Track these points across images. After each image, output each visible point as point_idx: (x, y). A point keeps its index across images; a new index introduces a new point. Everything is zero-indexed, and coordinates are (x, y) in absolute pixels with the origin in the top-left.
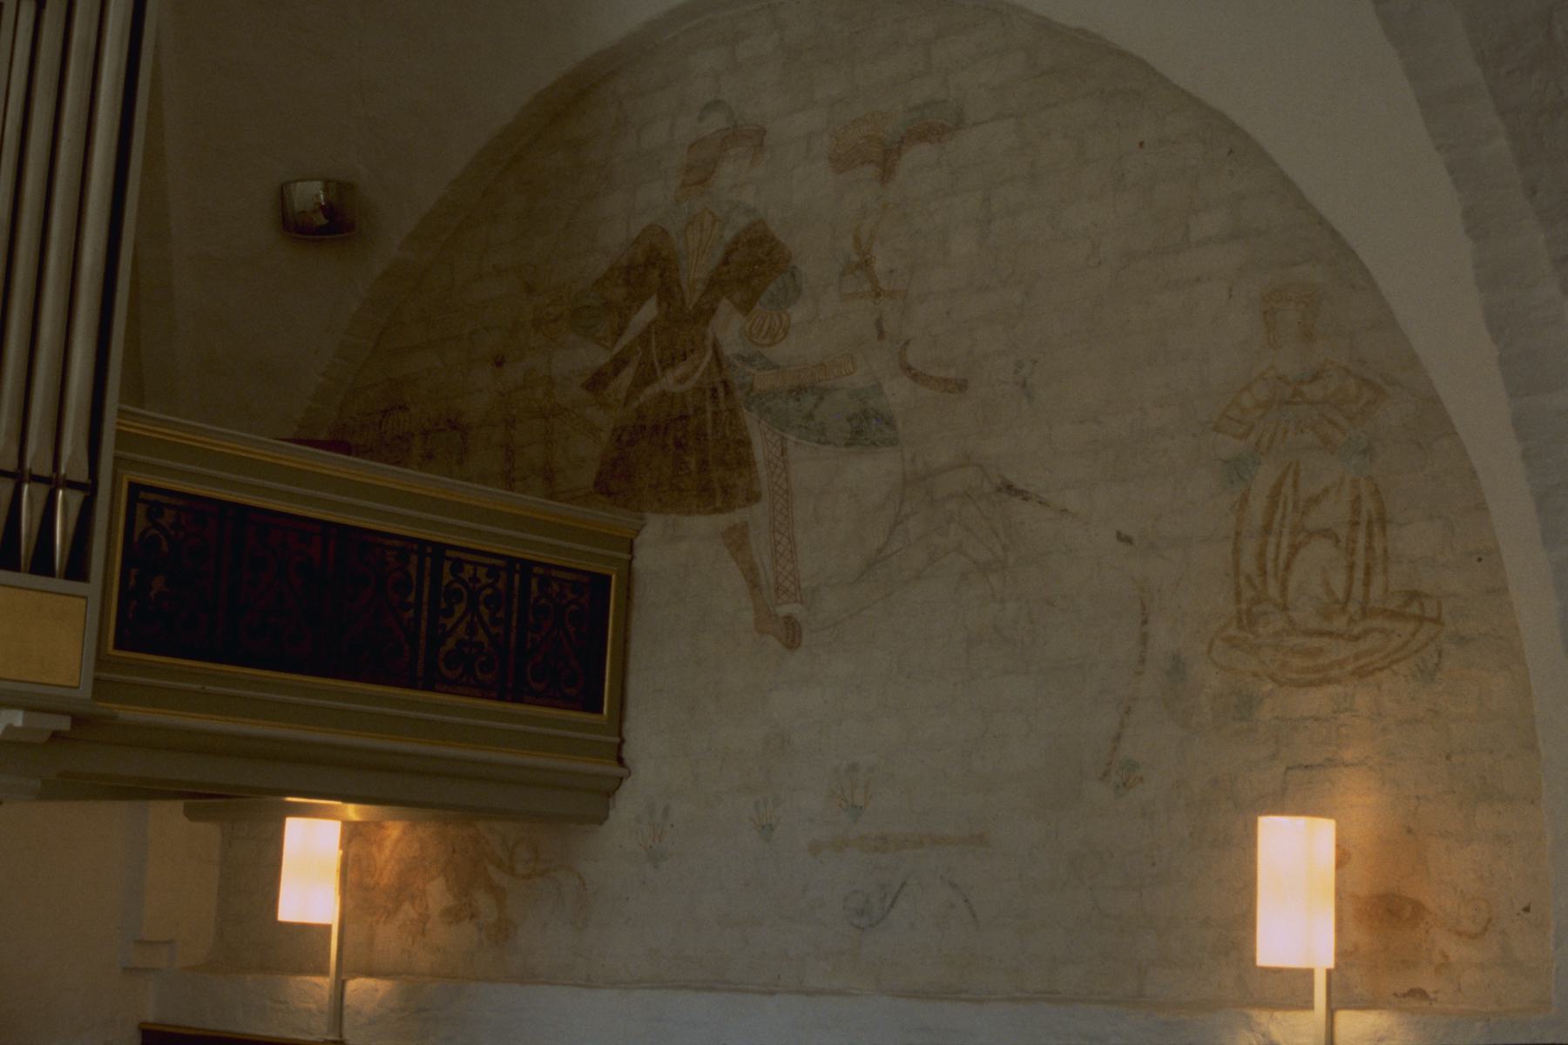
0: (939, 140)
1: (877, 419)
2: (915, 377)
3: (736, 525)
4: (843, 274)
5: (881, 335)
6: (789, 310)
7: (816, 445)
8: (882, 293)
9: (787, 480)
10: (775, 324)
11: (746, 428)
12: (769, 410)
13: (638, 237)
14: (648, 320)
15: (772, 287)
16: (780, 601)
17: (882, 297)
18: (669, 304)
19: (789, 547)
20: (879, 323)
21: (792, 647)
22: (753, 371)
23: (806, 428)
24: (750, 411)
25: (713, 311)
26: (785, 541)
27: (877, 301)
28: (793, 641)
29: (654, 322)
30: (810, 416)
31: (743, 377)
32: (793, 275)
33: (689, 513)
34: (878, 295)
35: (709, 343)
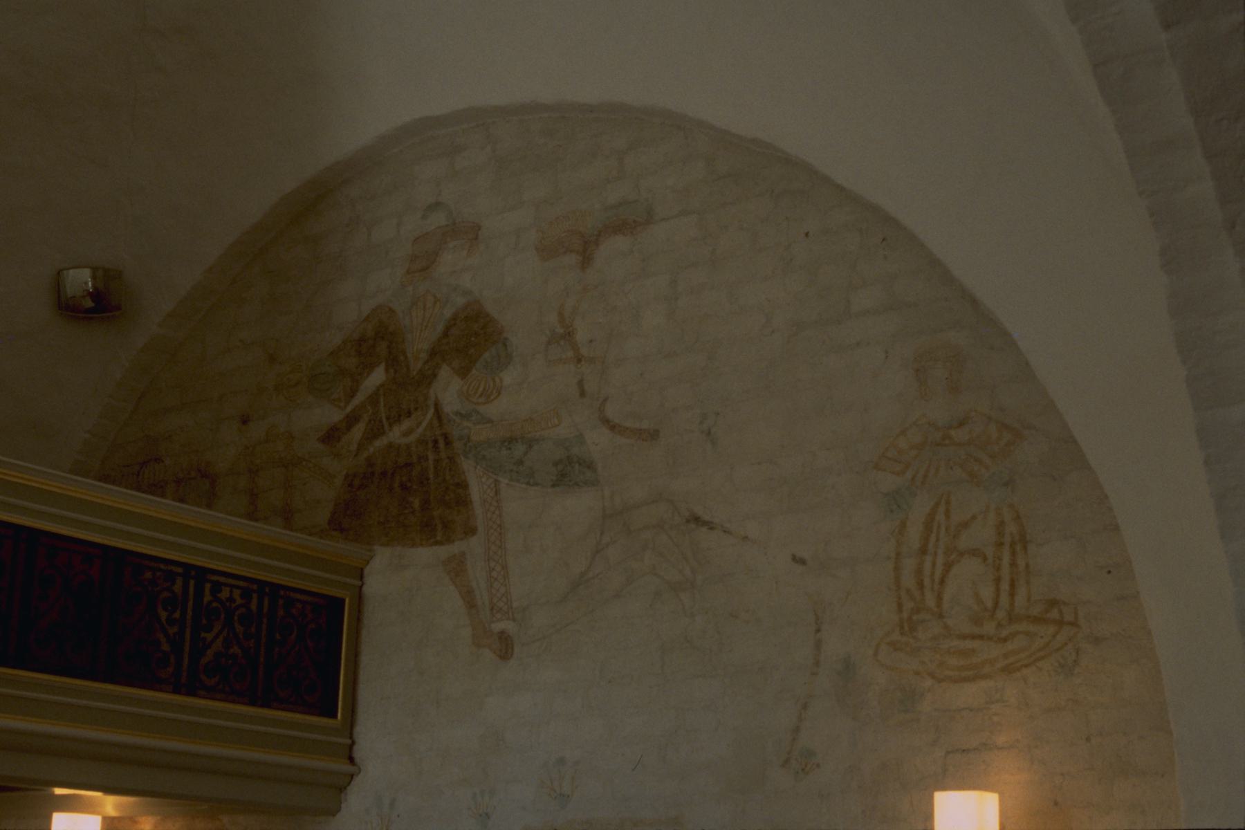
1: (580, 464)
2: (613, 428)
5: (583, 394)
7: (524, 486)
15: (487, 355)
17: (583, 363)
18: (396, 372)
20: (580, 384)
23: (517, 472)
25: (435, 376)
27: (579, 366)
29: (382, 385)
30: (520, 462)
32: (505, 345)
34: (579, 361)
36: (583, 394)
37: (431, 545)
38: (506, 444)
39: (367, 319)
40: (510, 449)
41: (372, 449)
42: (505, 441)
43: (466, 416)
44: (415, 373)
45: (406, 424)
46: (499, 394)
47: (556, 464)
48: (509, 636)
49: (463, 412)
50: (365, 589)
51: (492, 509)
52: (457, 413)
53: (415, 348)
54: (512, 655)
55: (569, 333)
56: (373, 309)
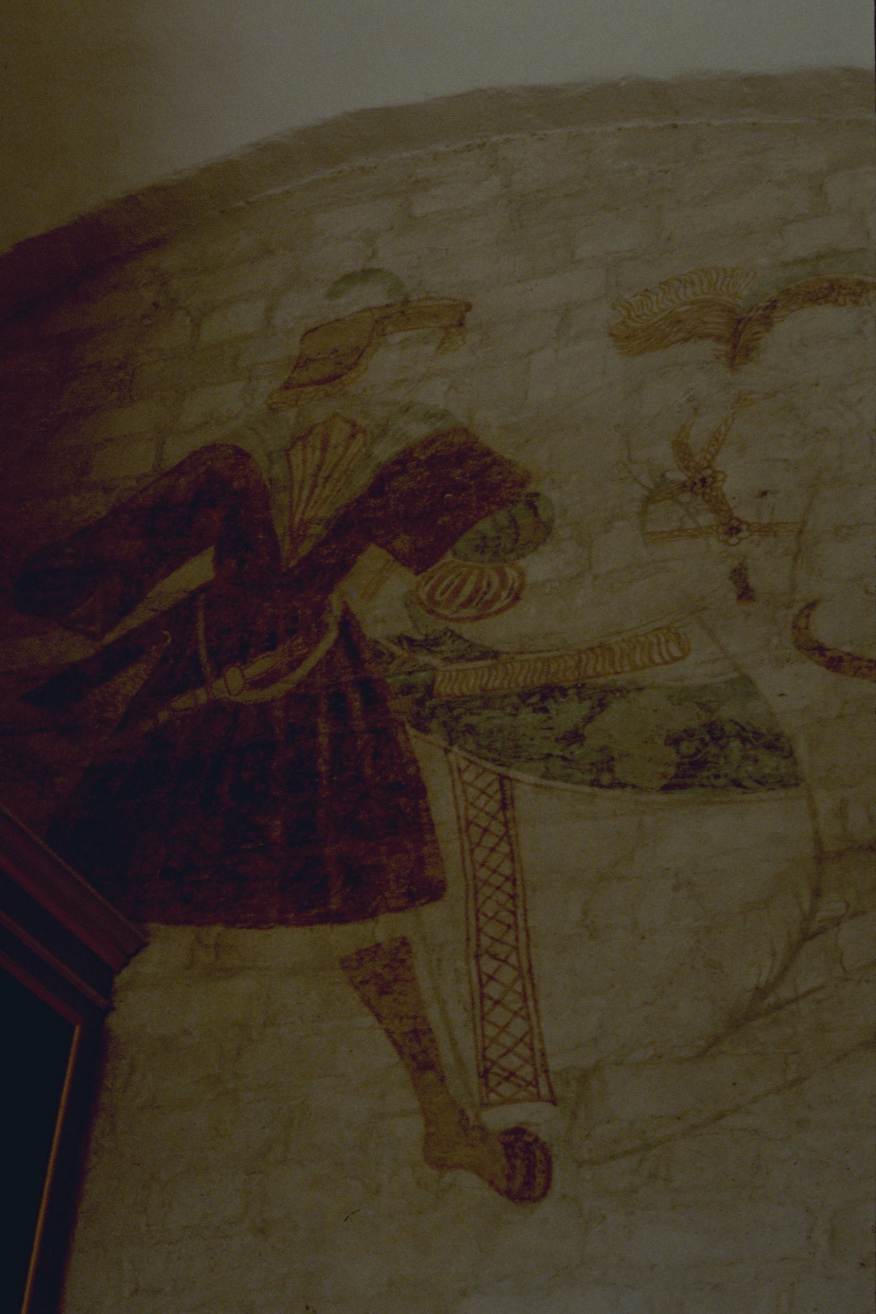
0: (856, 303)
1: (744, 740)
2: (835, 663)
3: (378, 945)
4: (649, 500)
5: (746, 594)
6: (522, 563)
7: (587, 789)
8: (744, 527)
9: (512, 857)
10: (489, 585)
11: (414, 761)
12: (470, 729)
13: (182, 464)
14: (193, 587)
15: (485, 526)
16: (493, 1097)
19: (518, 987)
20: (739, 575)
21: (522, 1199)
22: (435, 662)
23: (564, 758)
24: (426, 731)
26: (507, 974)
27: (734, 540)
28: (528, 1183)
29: (202, 589)
30: (576, 736)
31: (410, 673)
32: (532, 506)
33: (260, 922)
35: (332, 619)
36: (746, 594)
37: (310, 923)
38: (534, 699)
39: (179, 469)
40: (545, 710)
41: (163, 716)
42: (531, 694)
43: (430, 644)
44: (293, 563)
45: (261, 665)
46: (517, 598)
47: (675, 741)
48: (537, 1140)
49: (418, 637)
50: (113, 1021)
51: (489, 841)
52: (400, 640)
53: (297, 519)
54: (547, 1187)
55: (703, 480)
56: (195, 453)
